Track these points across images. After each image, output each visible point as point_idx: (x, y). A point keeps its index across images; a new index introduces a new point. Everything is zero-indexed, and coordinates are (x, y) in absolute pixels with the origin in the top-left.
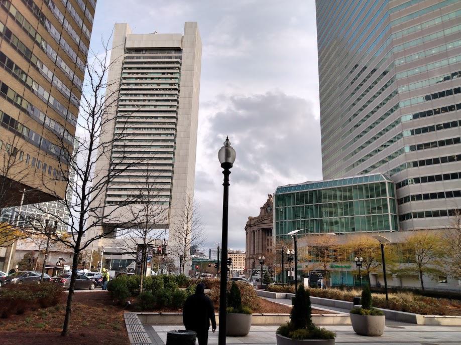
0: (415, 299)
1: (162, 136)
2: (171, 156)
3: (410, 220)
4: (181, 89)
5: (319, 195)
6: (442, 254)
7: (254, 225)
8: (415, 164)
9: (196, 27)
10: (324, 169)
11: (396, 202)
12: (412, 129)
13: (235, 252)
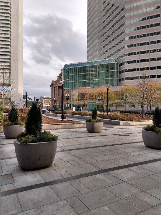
1: (2, 35)
2: (9, 47)
3: (124, 81)
4: (12, 6)
5: (84, 69)
6: (134, 96)
7: (54, 85)
8: (129, 54)
11: (118, 72)
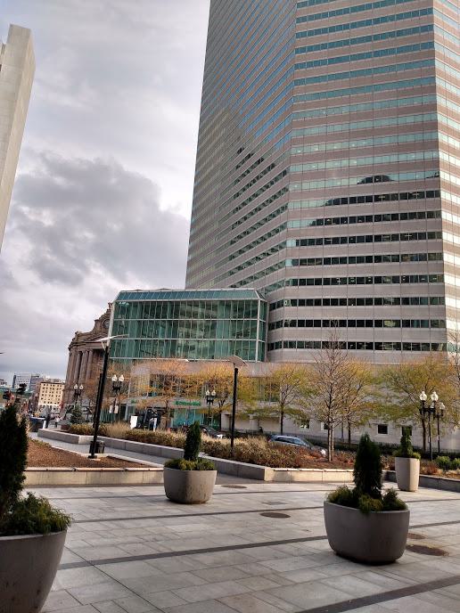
0: (268, 446)
7: (83, 344)
8: (295, 283)
9: (28, 37)
10: (189, 276)
11: (267, 326)
12: (298, 238)
13: (52, 381)
